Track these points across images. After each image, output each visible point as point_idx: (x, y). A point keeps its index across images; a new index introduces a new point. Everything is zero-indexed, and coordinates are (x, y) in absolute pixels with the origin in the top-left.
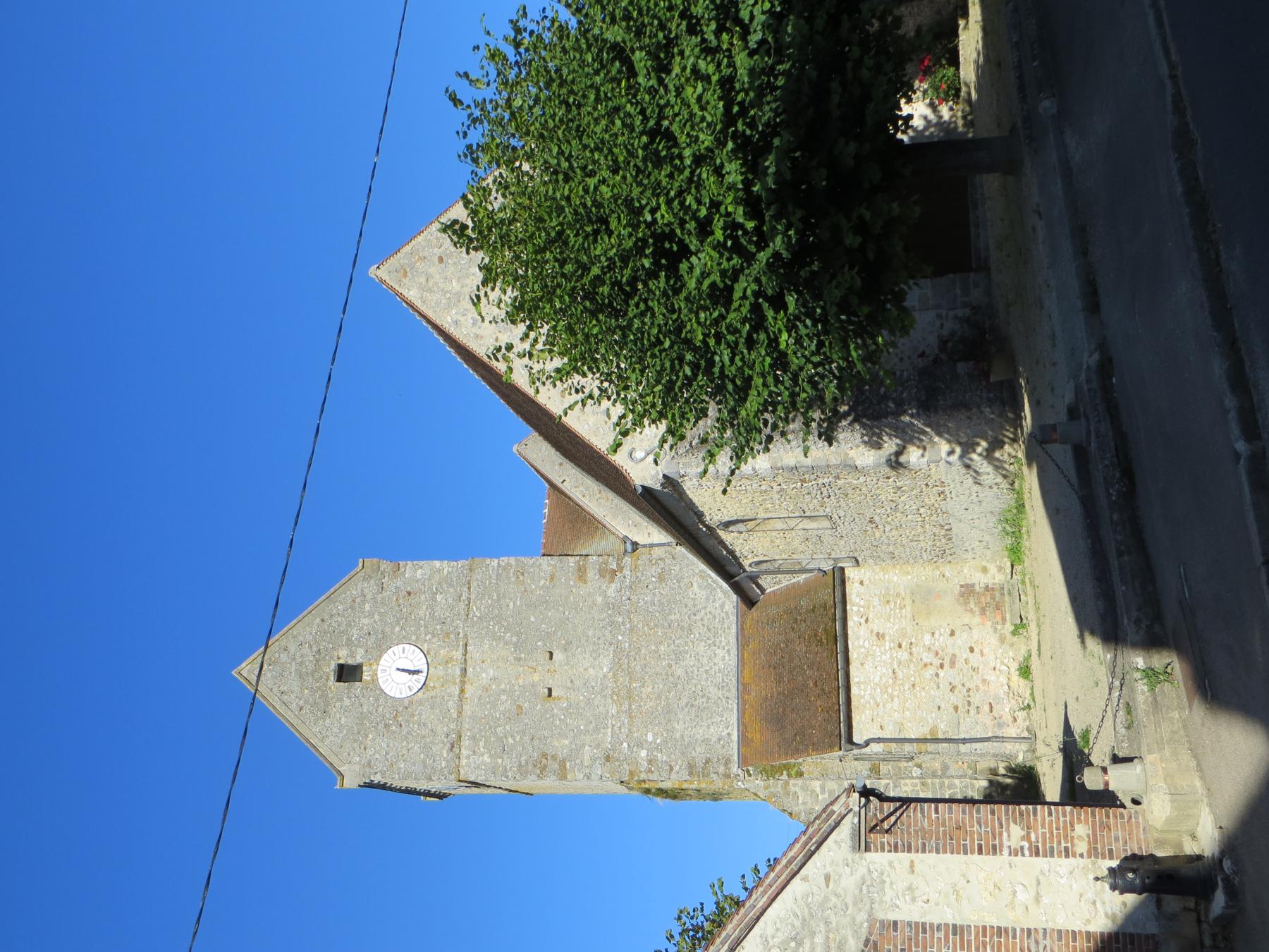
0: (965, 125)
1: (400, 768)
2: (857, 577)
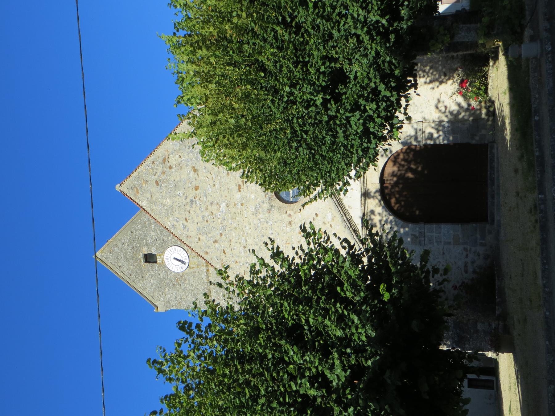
0: (487, 114)
1: (183, 305)
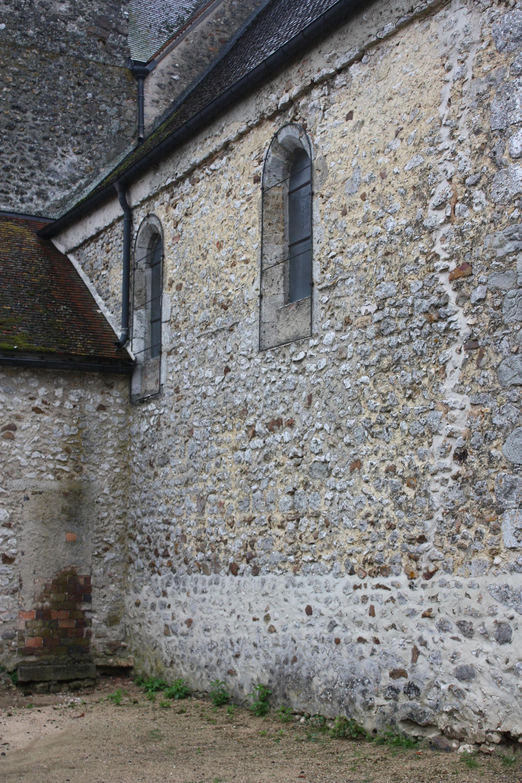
2: (112, 401)
